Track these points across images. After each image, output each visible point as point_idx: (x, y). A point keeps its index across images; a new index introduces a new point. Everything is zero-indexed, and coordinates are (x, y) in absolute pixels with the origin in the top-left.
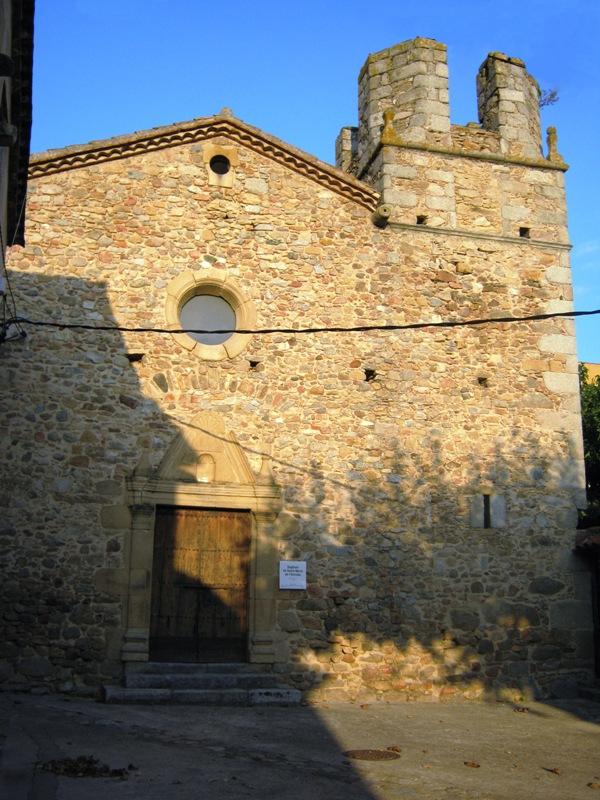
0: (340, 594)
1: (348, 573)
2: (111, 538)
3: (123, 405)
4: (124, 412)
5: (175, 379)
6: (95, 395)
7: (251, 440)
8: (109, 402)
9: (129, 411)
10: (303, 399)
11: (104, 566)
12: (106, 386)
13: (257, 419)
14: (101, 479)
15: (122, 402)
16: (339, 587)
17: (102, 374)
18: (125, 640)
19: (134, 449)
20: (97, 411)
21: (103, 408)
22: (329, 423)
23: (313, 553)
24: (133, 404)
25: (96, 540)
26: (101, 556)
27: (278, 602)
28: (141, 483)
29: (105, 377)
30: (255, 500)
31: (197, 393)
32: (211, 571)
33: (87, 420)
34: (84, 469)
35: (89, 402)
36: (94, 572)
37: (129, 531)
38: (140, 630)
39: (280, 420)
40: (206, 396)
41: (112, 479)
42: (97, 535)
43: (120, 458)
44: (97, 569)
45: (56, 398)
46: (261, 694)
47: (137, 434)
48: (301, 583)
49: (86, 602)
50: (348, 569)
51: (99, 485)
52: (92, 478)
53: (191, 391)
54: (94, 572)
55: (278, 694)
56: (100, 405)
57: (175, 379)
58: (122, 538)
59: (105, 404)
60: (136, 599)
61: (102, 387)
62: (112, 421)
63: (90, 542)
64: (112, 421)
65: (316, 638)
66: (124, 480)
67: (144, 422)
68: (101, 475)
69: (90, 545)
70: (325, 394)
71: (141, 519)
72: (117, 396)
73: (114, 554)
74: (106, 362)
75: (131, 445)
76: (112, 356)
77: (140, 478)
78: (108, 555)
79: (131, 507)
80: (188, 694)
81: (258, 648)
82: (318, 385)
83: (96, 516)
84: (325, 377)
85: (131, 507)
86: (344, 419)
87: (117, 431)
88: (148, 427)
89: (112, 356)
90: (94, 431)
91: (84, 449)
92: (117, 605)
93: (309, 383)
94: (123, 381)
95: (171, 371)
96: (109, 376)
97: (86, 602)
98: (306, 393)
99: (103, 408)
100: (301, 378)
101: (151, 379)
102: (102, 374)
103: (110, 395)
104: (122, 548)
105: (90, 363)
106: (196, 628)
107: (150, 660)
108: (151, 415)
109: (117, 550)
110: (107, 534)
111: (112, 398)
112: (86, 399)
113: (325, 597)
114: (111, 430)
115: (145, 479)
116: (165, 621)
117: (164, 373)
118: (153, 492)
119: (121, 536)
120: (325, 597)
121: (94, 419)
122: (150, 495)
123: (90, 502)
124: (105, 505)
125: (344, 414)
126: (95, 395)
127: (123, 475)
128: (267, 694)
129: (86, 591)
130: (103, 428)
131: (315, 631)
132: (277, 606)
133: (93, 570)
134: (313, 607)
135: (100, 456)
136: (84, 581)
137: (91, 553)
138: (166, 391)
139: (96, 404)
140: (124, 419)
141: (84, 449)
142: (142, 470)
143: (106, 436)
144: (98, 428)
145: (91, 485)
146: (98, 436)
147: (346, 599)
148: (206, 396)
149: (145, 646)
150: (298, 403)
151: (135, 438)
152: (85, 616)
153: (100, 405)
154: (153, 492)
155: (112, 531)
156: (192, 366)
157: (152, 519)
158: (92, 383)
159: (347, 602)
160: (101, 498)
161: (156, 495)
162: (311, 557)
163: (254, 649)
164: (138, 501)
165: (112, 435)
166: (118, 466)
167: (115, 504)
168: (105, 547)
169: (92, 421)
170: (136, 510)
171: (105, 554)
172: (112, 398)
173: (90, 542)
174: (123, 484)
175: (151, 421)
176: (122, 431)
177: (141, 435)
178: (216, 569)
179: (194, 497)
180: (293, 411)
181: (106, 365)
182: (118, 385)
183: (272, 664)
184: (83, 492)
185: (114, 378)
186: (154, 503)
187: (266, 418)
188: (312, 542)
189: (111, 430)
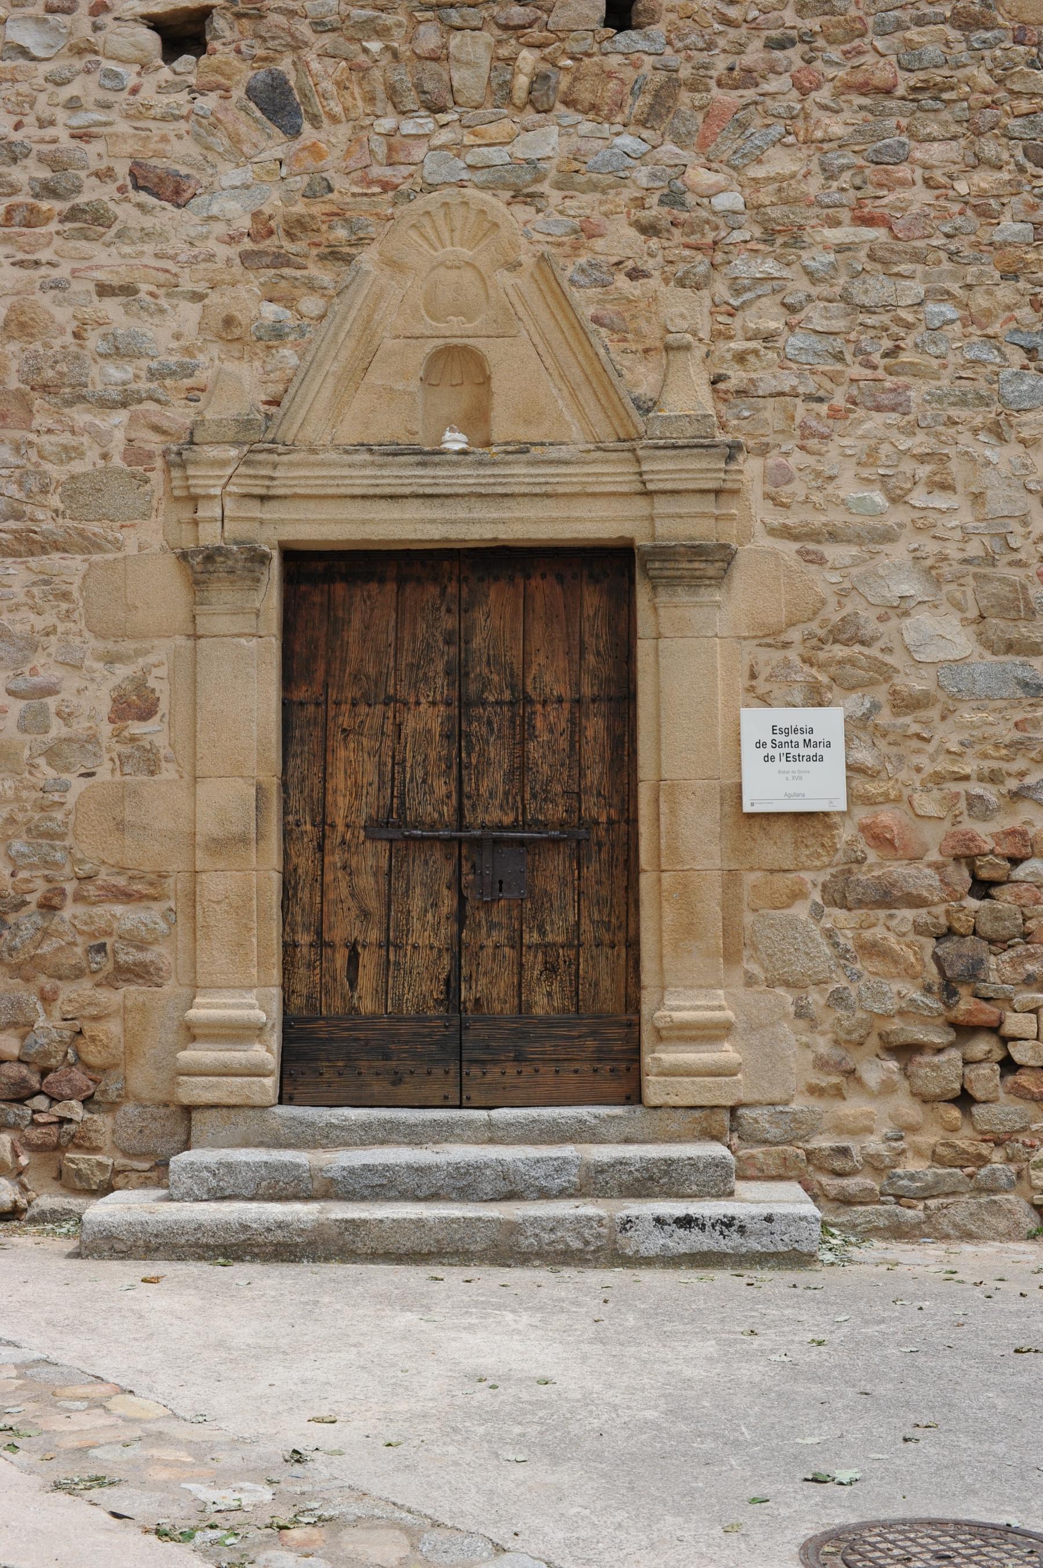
0: (989, 845)
1: (1020, 764)
2: (123, 671)
3: (143, 197)
4: (148, 222)
5: (327, 85)
6: (44, 174)
7: (621, 281)
8: (92, 193)
9: (165, 214)
10: (816, 113)
11: (104, 773)
12: (82, 135)
13: (640, 203)
14: (78, 467)
15: (137, 187)
16: (984, 818)
17: (65, 93)
18: (191, 1034)
19: (188, 351)
20: (54, 226)
21: (74, 214)
22: (920, 197)
23: (881, 693)
24: (177, 192)
25: (71, 683)
26: (93, 739)
27: (751, 878)
28: (216, 471)
29: (73, 105)
30: (640, 507)
31: (409, 127)
32: (499, 777)
33: (21, 264)
34: (18, 434)
35: (23, 198)
36: (71, 798)
37: (181, 641)
38: (249, 1001)
39: (730, 200)
40: (444, 137)
41: (117, 461)
42: (77, 667)
43: (144, 386)
44: (78, 785)
45: (943, 180)
46: (659, 1221)
47: (197, 297)
48: (823, 787)
49: (48, 906)
50: (1017, 747)
51: (72, 488)
52: (47, 466)
53: (386, 124)
54: (71, 798)
55: (728, 1223)
56: (60, 206)
57: (327, 85)
58: (162, 672)
59: (81, 200)
60: (219, 884)
61: (66, 142)
62: (107, 260)
63: (49, 691)
64: (107, 260)
65: (901, 1013)
66: (159, 463)
67: (223, 251)
68: (78, 453)
69: (52, 702)
70: (900, 91)
71: (224, 596)
72: (122, 169)
73: (136, 728)
74: (79, 51)
75: (177, 337)
76: (96, 28)
77: (212, 452)
78: (117, 735)
79: (184, 556)
80: (536, 1221)
81: (671, 1056)
82: (869, 59)
83: (65, 596)
84: (900, 26)
85: (184, 556)
86: (984, 179)
87: (128, 290)
88: (237, 269)
89: (96, 28)
90: (45, 300)
91: (14, 365)
92: (158, 907)
93: (835, 53)
94: (138, 114)
95: (310, 56)
96: (88, 101)
97: (48, 906)
98: (823, 95)
99: (74, 214)
100: (807, 38)
101: (238, 93)
102: (65, 93)
103: (95, 165)
104: (163, 707)
105: (22, 62)
106: (451, 985)
107: (283, 1099)
108: (245, 223)
109: (146, 714)
110: (111, 659)
111: (105, 175)
112: (14, 190)
113: (934, 856)
114: (104, 290)
115: (233, 453)
116: (341, 959)
117: (285, 65)
118: (263, 498)
119: (158, 663)
120: (934, 856)
121: (44, 255)
122: (255, 510)
123: (44, 551)
124: (96, 557)
125: (980, 162)
126: (44, 174)
127: (154, 443)
128: (686, 1222)
129: (47, 864)
130: (76, 286)
131: (896, 986)
132: (746, 894)
133: (65, 788)
134: (887, 898)
135: (61, 389)
136: (36, 832)
137: (57, 729)
138: (294, 132)
139: (45, 205)
140: (149, 248)
141: (14, 365)
142: (219, 423)
143: (88, 312)
144: (57, 286)
145: (44, 490)
146: (62, 315)
147: (1015, 861)
148: (444, 137)
149: (266, 1053)
150: (794, 129)
151: (191, 312)
152: (46, 948)
153: (60, 206)
154: (263, 498)
155: (128, 646)
156: (382, 32)
157: (269, 596)
158: (31, 130)
159: (1021, 872)
160: (81, 533)
161: (271, 512)
162: (876, 707)
163: (659, 1057)
164: (210, 535)
165: (111, 308)
166: (133, 420)
167: (131, 549)
168: (105, 707)
169: (37, 263)
170: (202, 567)
171: (106, 729)
172: (105, 175)
173: (49, 691)
174: (156, 477)
175: (247, 244)
176: (144, 287)
177: (214, 298)
178: (521, 769)
179: (414, 511)
180: (781, 163)
181: (79, 64)
182: (123, 127)
183: (733, 1110)
184: (18, 516)
185: (107, 106)
186: (268, 540)
187: (673, 199)
188: (874, 651)
189: (104, 290)
